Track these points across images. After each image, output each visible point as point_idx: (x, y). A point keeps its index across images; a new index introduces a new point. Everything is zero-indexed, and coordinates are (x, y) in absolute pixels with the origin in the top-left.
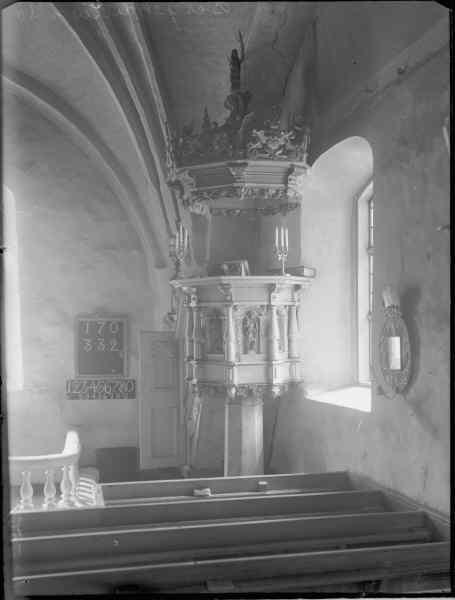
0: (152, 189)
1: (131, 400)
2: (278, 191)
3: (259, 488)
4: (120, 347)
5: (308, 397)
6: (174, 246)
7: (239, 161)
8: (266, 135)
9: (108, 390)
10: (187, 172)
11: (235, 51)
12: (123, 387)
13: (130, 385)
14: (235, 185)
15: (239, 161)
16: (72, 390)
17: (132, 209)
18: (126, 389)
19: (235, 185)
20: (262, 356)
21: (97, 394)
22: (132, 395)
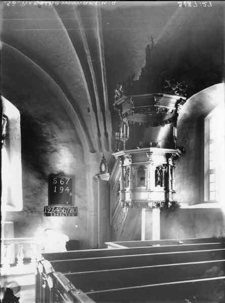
0: (92, 112)
1: (75, 217)
2: (173, 111)
3: (179, 244)
4: (71, 191)
5: (181, 208)
6: (119, 136)
7: (159, 94)
8: (171, 83)
9: (64, 211)
10: (131, 98)
11: (148, 46)
12: (72, 211)
13: (75, 210)
14: (155, 105)
15: (159, 94)
16: (47, 212)
17: (78, 123)
18: (73, 211)
19: (155, 105)
20: (163, 188)
21: (59, 214)
22: (76, 215)
